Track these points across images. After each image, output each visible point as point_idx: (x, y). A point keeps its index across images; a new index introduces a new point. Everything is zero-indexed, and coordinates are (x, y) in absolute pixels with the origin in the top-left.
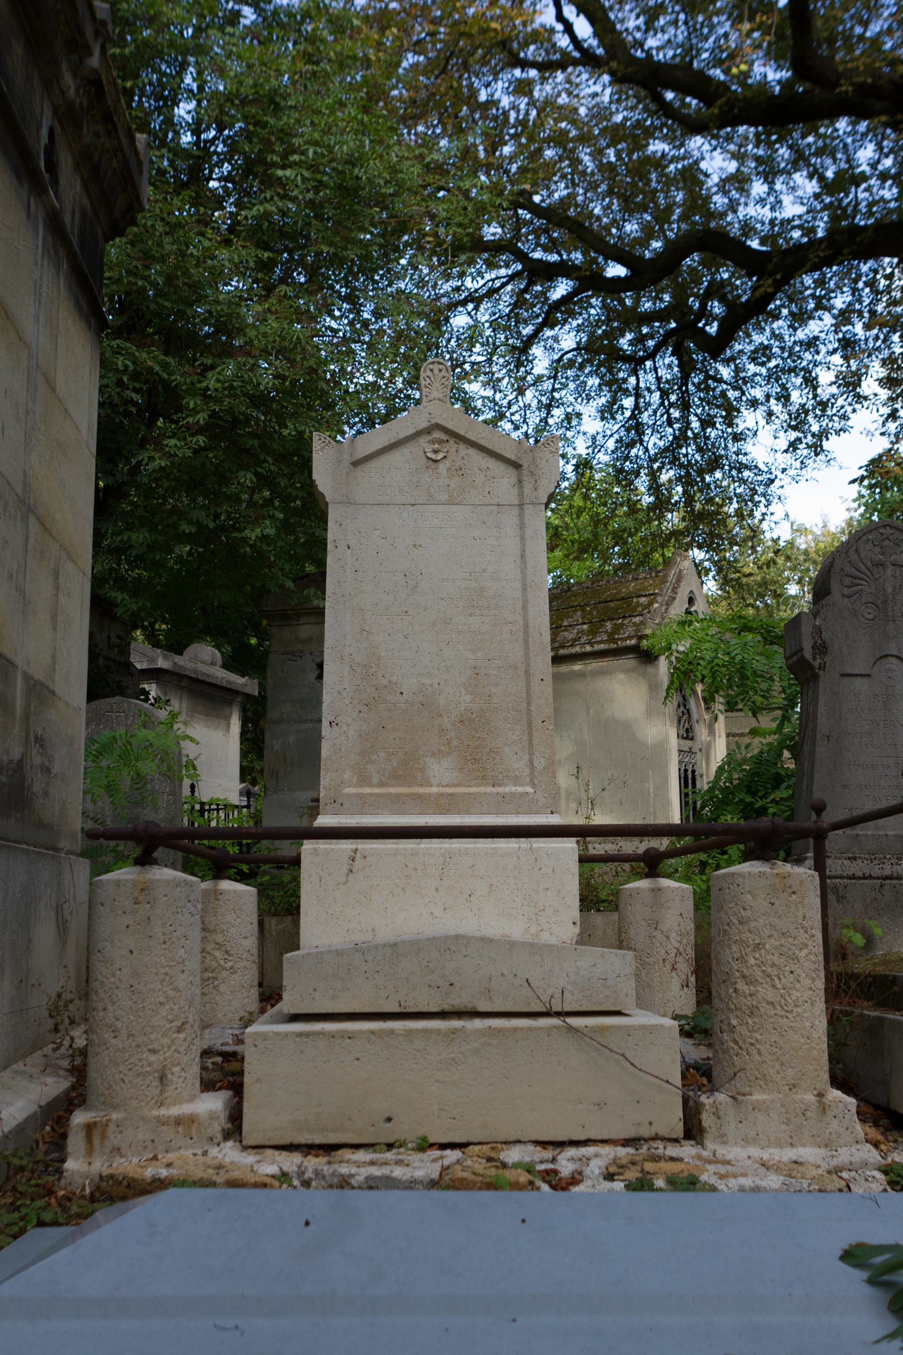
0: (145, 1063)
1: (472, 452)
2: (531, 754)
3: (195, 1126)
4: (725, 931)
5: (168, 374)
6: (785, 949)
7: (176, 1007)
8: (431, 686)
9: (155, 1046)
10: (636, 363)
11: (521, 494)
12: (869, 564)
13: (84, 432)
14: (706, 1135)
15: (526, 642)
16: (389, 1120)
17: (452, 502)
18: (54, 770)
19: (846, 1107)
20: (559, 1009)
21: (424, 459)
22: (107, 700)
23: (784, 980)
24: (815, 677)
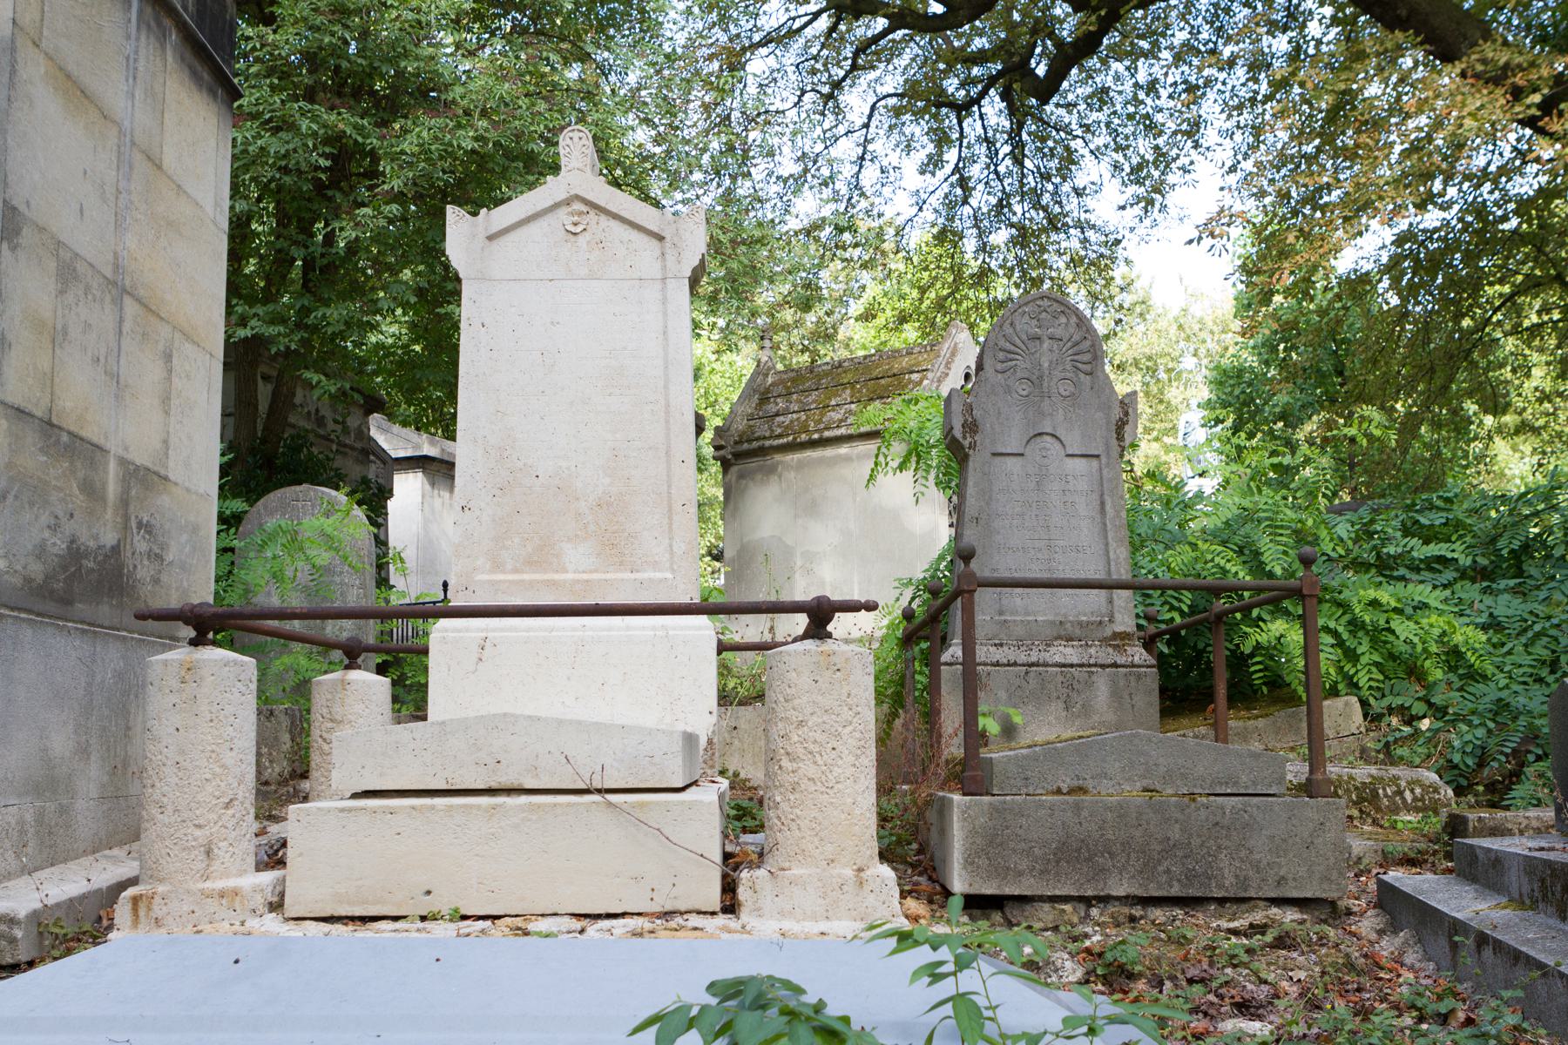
1: (614, 224)
9: (202, 822)
10: (963, 109)
11: (664, 268)
12: (1024, 337)
13: (209, 209)
15: (667, 422)
16: (429, 893)
17: (592, 277)
18: (169, 557)
24: (966, 456)
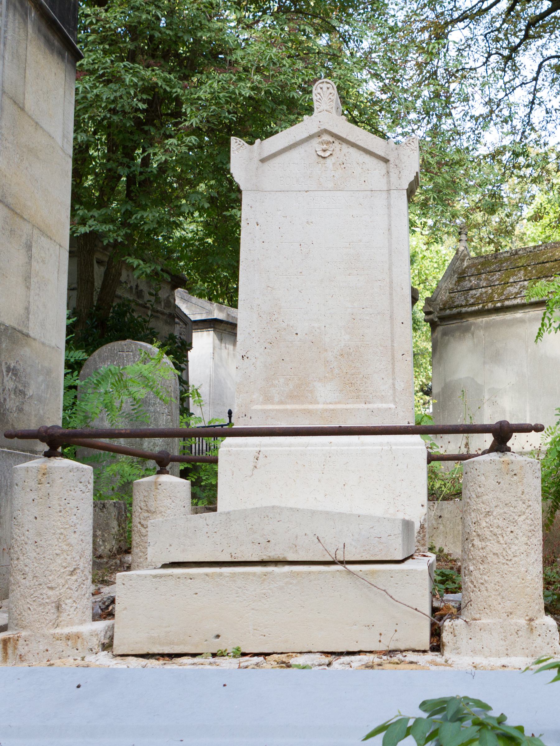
0: (45, 596)
1: (352, 150)
2: (394, 379)
3: (80, 640)
4: (468, 503)
5: (171, 88)
6: (507, 516)
7: (69, 558)
8: (319, 328)
9: (53, 585)
11: (389, 182)
13: (59, 140)
14: (445, 648)
15: (391, 294)
16: (218, 636)
17: (336, 189)
18: (30, 392)
19: (548, 628)
20: (342, 559)
21: (316, 156)
22: (120, 342)
23: (506, 538)
